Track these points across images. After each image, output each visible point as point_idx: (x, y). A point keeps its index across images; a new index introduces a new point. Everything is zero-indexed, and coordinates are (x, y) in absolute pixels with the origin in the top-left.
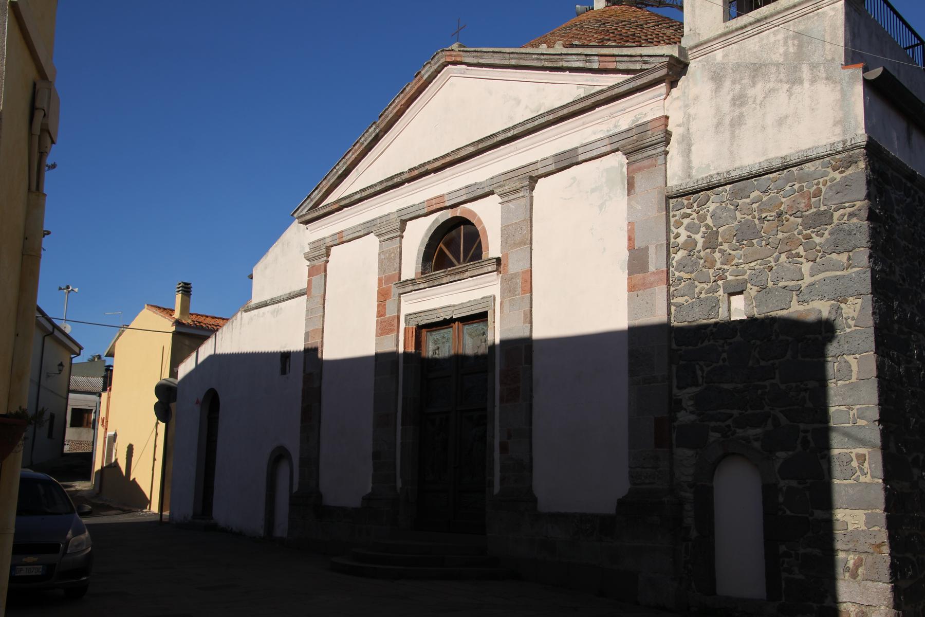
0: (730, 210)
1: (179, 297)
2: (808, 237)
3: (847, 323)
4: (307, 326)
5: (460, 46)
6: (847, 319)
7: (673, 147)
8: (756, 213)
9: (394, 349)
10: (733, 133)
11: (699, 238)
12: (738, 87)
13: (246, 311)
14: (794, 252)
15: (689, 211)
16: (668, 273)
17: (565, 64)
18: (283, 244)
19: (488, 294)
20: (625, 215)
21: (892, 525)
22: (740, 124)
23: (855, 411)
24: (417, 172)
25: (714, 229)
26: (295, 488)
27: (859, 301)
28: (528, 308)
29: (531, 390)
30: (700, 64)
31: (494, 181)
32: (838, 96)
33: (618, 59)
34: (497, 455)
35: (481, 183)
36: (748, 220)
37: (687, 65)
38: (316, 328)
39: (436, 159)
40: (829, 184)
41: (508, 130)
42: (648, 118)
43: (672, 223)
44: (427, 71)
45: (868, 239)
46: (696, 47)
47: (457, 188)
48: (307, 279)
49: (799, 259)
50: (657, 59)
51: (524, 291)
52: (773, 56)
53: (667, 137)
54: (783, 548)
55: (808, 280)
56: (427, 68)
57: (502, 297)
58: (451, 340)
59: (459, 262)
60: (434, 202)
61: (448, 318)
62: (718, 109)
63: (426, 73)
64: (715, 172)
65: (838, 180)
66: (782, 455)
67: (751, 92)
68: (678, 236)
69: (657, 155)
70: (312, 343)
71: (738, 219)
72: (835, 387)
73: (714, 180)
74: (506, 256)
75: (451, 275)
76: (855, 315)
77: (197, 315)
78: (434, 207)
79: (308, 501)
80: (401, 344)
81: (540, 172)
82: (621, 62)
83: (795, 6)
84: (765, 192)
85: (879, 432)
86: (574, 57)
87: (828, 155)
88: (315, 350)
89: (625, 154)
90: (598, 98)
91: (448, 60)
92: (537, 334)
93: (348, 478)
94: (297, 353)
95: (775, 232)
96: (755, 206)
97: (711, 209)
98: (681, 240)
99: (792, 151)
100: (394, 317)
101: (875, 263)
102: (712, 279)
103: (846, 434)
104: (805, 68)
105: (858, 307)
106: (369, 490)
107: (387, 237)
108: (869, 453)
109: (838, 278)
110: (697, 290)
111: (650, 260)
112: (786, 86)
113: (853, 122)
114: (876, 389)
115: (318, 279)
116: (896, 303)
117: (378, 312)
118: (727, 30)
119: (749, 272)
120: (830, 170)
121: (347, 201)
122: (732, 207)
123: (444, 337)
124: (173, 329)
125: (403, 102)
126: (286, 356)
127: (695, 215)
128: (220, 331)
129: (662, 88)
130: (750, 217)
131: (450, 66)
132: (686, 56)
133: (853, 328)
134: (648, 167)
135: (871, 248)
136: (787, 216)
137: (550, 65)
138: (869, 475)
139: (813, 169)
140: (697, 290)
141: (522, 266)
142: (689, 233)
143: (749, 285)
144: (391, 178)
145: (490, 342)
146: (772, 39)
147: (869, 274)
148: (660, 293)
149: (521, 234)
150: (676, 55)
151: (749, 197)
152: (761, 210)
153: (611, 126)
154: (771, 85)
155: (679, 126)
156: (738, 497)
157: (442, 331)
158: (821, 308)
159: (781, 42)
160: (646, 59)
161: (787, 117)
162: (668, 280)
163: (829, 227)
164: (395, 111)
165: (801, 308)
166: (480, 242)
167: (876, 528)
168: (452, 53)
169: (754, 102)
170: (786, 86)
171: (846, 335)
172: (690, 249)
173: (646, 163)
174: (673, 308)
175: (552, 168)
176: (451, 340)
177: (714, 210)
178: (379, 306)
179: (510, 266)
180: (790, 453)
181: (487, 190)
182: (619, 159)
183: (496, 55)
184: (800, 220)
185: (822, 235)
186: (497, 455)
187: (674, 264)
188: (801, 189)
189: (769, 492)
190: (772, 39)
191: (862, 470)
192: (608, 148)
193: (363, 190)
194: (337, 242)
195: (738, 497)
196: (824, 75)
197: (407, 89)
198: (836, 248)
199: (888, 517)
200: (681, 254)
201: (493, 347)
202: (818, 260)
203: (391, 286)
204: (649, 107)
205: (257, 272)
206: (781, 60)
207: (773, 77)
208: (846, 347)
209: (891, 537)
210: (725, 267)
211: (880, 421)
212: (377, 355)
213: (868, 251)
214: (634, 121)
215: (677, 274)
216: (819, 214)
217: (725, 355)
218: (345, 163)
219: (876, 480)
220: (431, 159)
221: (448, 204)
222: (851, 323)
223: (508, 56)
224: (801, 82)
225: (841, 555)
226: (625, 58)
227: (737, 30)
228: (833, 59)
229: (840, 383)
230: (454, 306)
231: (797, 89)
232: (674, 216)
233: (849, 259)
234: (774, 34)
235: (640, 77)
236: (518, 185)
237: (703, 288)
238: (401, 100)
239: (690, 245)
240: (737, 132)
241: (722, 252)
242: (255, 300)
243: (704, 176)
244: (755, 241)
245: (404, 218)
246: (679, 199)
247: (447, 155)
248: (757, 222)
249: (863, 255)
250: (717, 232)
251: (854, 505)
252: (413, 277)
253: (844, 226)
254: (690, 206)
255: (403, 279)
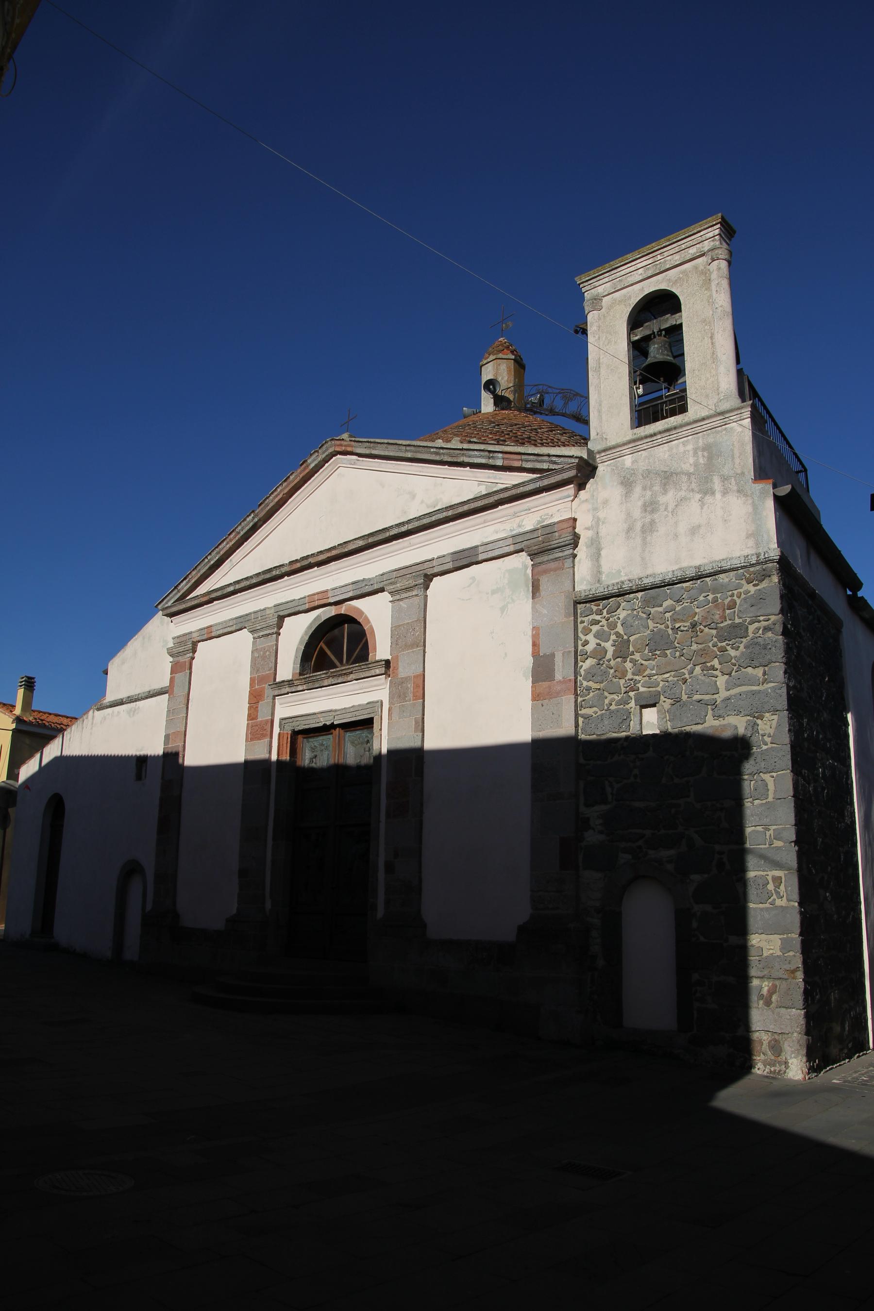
0: (641, 618)
1: (21, 692)
2: (723, 650)
3: (763, 740)
4: (167, 728)
5: (350, 436)
6: (763, 736)
7: (582, 551)
8: (669, 623)
9: (266, 756)
10: (644, 539)
11: (609, 646)
12: (649, 493)
13: (98, 709)
14: (709, 665)
15: (598, 618)
16: (576, 682)
17: (466, 460)
18: (144, 638)
19: (375, 699)
20: (530, 618)
21: (806, 949)
22: (652, 531)
23: (771, 832)
24: (298, 565)
25: (625, 637)
26: (149, 907)
27: (776, 717)
28: (420, 716)
29: (422, 805)
30: (609, 469)
31: (385, 577)
32: (750, 509)
33: (524, 457)
34: (381, 875)
35: (370, 580)
36: (660, 629)
37: (595, 468)
38: (178, 728)
39: (321, 552)
40: (743, 596)
41: (402, 524)
42: (555, 520)
43: (580, 630)
44: (314, 460)
45: (783, 654)
46: (605, 450)
47: (342, 584)
48: (169, 676)
49: (714, 672)
50: (566, 460)
51: (416, 697)
52: (683, 466)
53: (575, 540)
54: (695, 976)
55: (723, 694)
56: (314, 456)
57: (391, 703)
58: (331, 748)
59: (341, 662)
60: (316, 597)
61: (328, 723)
62: (629, 515)
63: (312, 462)
64: (626, 578)
65: (752, 593)
66: (696, 877)
67: (662, 499)
68: (586, 643)
69: (565, 558)
70: (173, 746)
71: (651, 627)
72: (751, 806)
73: (626, 587)
74: (396, 658)
75: (333, 677)
76: (771, 732)
77: (40, 712)
78: (316, 603)
79: (163, 921)
80: (273, 750)
81: (436, 570)
82: (527, 461)
83: (703, 419)
84: (678, 601)
85: (795, 853)
86: (476, 453)
87: (742, 568)
88: (175, 755)
89: (529, 555)
90: (502, 496)
91: (338, 449)
92: (430, 744)
93: (210, 898)
94: (155, 758)
95: (689, 643)
96: (668, 615)
97: (621, 617)
98: (590, 648)
99: (706, 561)
100: (267, 721)
101: (789, 679)
102: (623, 690)
103: (762, 857)
104: (716, 480)
105: (774, 723)
106: (234, 911)
107: (262, 633)
108: (785, 875)
109: (754, 693)
110: (607, 701)
111: (556, 667)
112: (698, 496)
113: (765, 536)
114: (792, 809)
115: (181, 677)
116: (806, 720)
117: (249, 715)
118: (635, 437)
119: (662, 684)
120: (744, 582)
121: (219, 594)
122: (644, 616)
123: (322, 745)
124: (14, 726)
125: (286, 491)
126: (142, 761)
127: (604, 622)
128: (69, 730)
129: (570, 489)
130: (663, 627)
131: (339, 456)
132: (594, 459)
133: (770, 745)
134: (555, 570)
135: (785, 664)
136: (702, 627)
137: (450, 459)
138: (785, 898)
139: (727, 580)
140: (607, 701)
141: (416, 670)
142: (598, 641)
143: (662, 697)
144: (270, 570)
145: (375, 751)
146: (682, 449)
147: (784, 690)
148: (567, 703)
149: (413, 635)
150: (585, 457)
151: (661, 606)
152: (675, 620)
153: (515, 526)
154: (683, 493)
155: (588, 529)
156: (649, 922)
157: (321, 738)
158: (736, 724)
159: (691, 452)
160: (554, 459)
161: (699, 526)
162: (576, 689)
163: (744, 640)
164: (276, 500)
165: (716, 723)
166: (367, 642)
167: (791, 953)
168: (342, 442)
169: (666, 509)
170: (698, 496)
171: (763, 753)
172: (599, 657)
173: (553, 565)
174: (581, 720)
175: (450, 566)
176: (331, 748)
177: (625, 618)
178: (250, 708)
179: (400, 669)
180: (706, 876)
181: (376, 587)
182: (522, 560)
183: (390, 447)
184: (714, 632)
185: (737, 649)
186: (381, 875)
187: (583, 673)
188: (715, 600)
189: (682, 917)
190: (682, 449)
191: (778, 893)
192: (512, 548)
193: (238, 582)
194: (205, 637)
195: (649, 922)
196: (735, 488)
197: (291, 477)
198: (752, 661)
199: (802, 942)
200: (590, 662)
201: (379, 757)
202: (733, 673)
203: (264, 687)
204: (559, 507)
205: (113, 667)
206: (692, 470)
207: (684, 486)
208: (762, 765)
209: (805, 963)
210: (637, 678)
211: (796, 842)
212: (247, 763)
213: (783, 667)
214: (539, 522)
215: (585, 683)
216: (734, 626)
217: (636, 771)
218: (219, 553)
219: (792, 903)
220: (315, 551)
221: (332, 600)
222: (768, 739)
223: (404, 448)
224: (713, 493)
225: (755, 983)
226: (531, 457)
227: (646, 437)
228: (743, 473)
229: (756, 802)
230: (336, 711)
231: (708, 499)
232: (582, 622)
233: (765, 674)
234: (684, 444)
235: (547, 477)
236: (411, 583)
237: (613, 700)
238: (282, 490)
239: (599, 654)
240: (649, 538)
241: (634, 662)
242: (110, 697)
243: (614, 581)
244: (668, 652)
245: (282, 613)
246: (588, 605)
247: (334, 548)
248: (670, 632)
249: (778, 670)
250: (629, 641)
251: (769, 930)
252: (290, 678)
253: (760, 640)
254: (600, 612)
255: (277, 680)
